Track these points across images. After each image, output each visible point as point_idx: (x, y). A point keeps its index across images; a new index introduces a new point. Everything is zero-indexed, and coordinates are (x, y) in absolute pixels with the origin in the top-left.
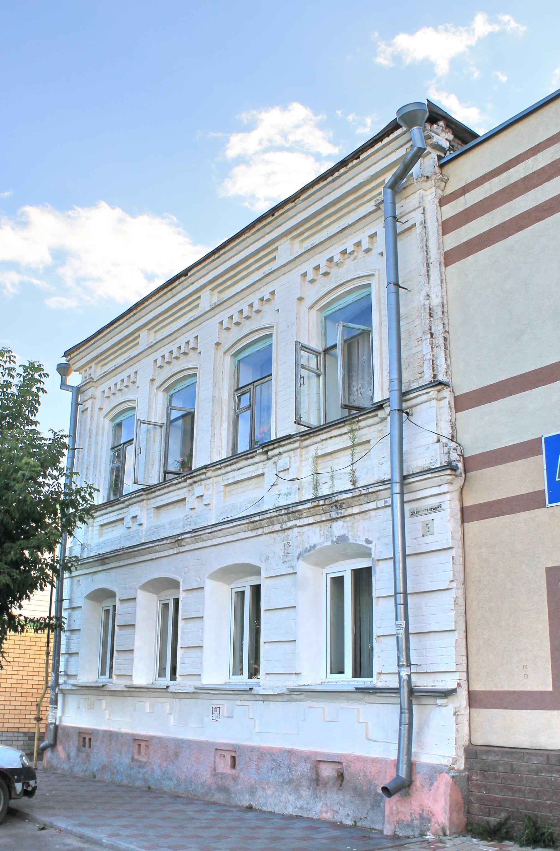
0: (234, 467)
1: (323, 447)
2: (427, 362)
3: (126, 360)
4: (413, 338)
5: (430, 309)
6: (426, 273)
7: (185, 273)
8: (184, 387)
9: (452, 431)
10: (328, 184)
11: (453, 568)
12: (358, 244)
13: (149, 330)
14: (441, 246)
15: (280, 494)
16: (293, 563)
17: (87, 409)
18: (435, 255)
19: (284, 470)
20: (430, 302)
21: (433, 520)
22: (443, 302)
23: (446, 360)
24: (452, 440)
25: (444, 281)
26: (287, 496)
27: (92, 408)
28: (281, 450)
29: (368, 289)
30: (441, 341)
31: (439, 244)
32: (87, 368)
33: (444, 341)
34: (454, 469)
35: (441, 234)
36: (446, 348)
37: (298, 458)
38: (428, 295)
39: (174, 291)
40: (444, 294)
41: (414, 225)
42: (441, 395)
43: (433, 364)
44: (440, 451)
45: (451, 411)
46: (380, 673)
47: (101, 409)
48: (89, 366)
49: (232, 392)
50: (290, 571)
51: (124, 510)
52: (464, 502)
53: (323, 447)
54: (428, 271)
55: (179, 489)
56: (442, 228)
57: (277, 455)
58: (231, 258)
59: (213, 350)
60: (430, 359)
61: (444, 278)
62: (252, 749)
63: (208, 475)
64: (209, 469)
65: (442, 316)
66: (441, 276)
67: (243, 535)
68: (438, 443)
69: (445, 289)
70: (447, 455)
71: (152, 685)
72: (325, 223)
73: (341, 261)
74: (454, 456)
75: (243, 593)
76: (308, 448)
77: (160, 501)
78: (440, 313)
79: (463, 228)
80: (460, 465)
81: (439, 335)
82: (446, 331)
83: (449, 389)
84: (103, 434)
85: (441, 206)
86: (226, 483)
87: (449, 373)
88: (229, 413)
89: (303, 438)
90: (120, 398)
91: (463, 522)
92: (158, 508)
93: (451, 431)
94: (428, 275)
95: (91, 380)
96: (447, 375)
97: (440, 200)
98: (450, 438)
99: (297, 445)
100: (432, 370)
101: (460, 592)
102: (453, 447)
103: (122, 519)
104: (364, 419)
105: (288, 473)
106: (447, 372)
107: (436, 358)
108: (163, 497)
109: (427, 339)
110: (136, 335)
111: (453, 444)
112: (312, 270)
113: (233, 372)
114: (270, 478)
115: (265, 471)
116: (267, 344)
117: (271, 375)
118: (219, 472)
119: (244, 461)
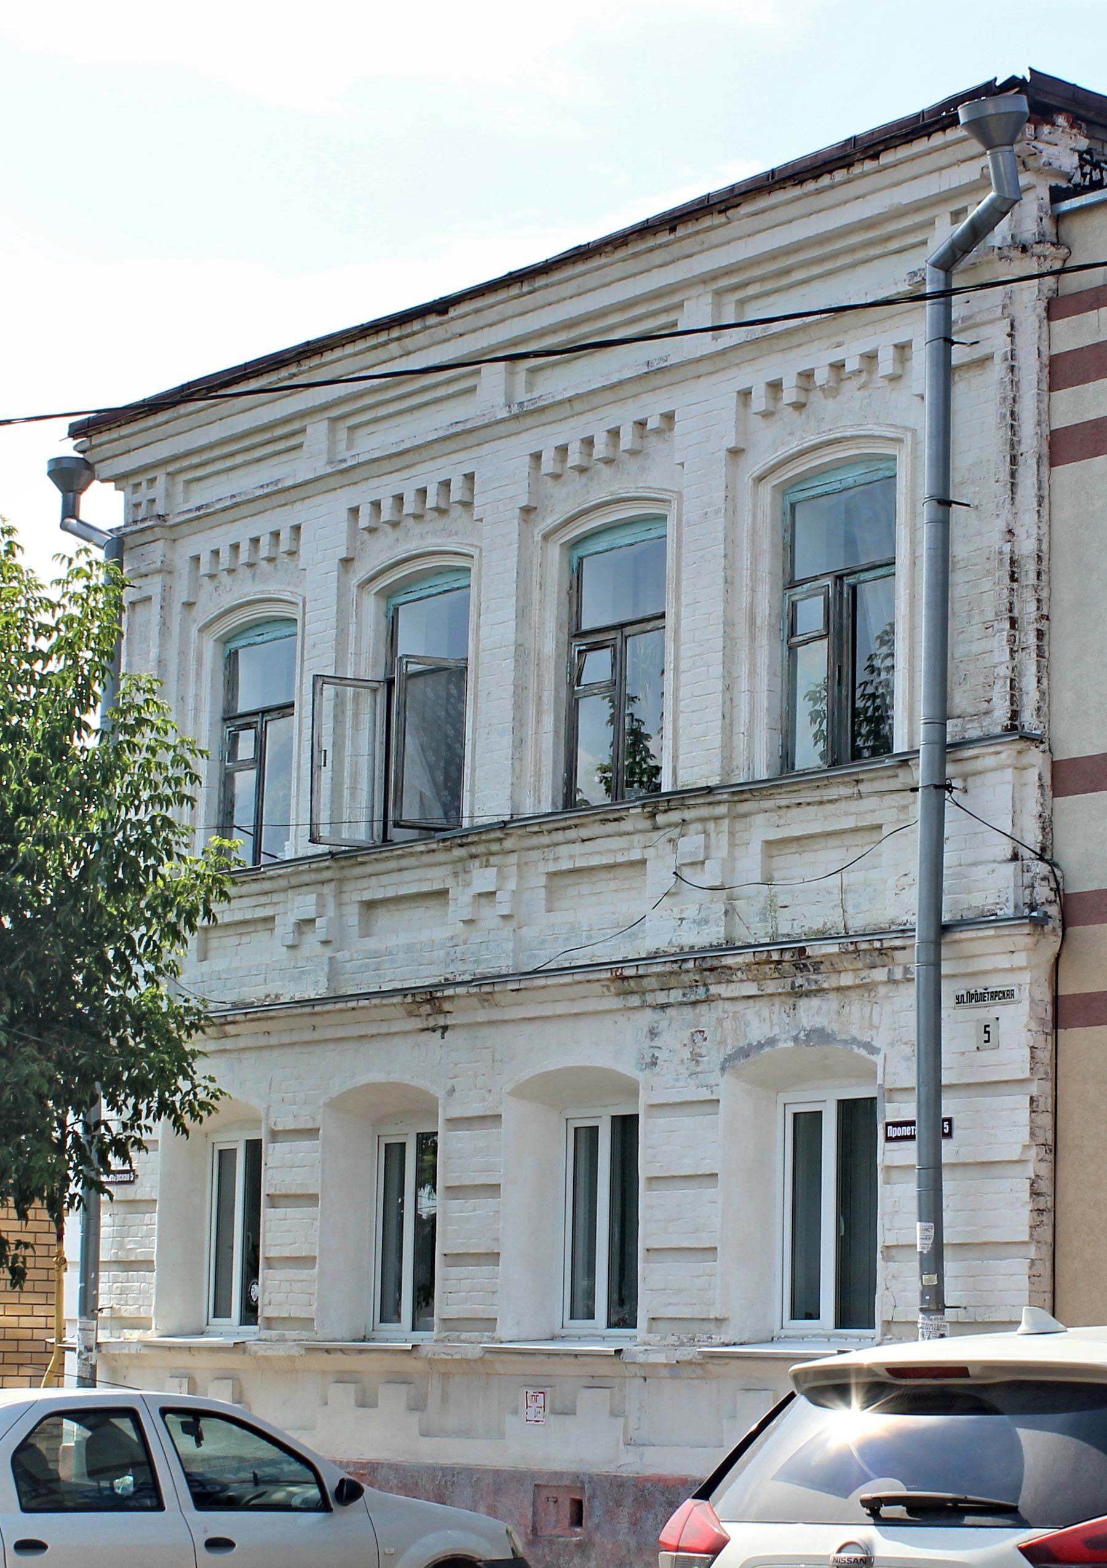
0: (572, 834)
1: (782, 822)
2: (1000, 682)
3: (266, 490)
4: (976, 619)
5: (1012, 562)
6: (1008, 478)
7: (441, 307)
8: (434, 591)
9: (1043, 836)
10: (807, 195)
11: (1032, 1121)
12: (871, 358)
13: (334, 420)
14: (1045, 417)
15: (684, 919)
16: (712, 1079)
17: (149, 599)
18: (1030, 441)
19: (693, 864)
20: (1013, 546)
21: (997, 1019)
22: (1040, 550)
23: (1039, 682)
24: (1041, 858)
25: (1046, 500)
26: (699, 924)
27: (163, 599)
28: (688, 814)
29: (890, 464)
30: (1031, 639)
31: (1039, 414)
32: (143, 478)
33: (1038, 639)
34: (1039, 923)
35: (1045, 387)
36: (1040, 654)
37: (724, 838)
38: (1010, 531)
39: (409, 343)
40: (1045, 529)
41: (989, 358)
42: (1026, 760)
43: (1012, 688)
44: (1015, 881)
45: (1042, 795)
46: (889, 1322)
47: (189, 605)
48: (150, 476)
49: (565, 638)
50: (705, 1095)
51: (276, 898)
52: (1059, 990)
53: (782, 822)
54: (1013, 475)
55: (430, 865)
56: (1050, 373)
57: (676, 825)
58: (565, 299)
59: (516, 521)
60: (1006, 677)
61: (1046, 493)
62: (617, 1484)
63: (508, 844)
64: (508, 831)
65: (1035, 582)
66: (1040, 489)
67: (592, 1005)
68: (1012, 865)
69: (1046, 518)
70: (1028, 891)
71: (363, 1341)
72: (797, 276)
73: (831, 384)
74: (1043, 892)
75: (594, 1130)
76: (748, 819)
77: (375, 890)
78: (1033, 575)
79: (1091, 386)
80: (1054, 910)
81: (1029, 623)
82: (1042, 617)
83: (1042, 747)
84: (198, 675)
85: (1050, 318)
86: (552, 867)
87: (1045, 709)
88: (557, 690)
89: (736, 799)
90: (246, 588)
91: (1056, 1026)
92: (370, 905)
93: (1041, 837)
94: (1012, 484)
95: (159, 522)
96: (1038, 716)
97: (1048, 303)
98: (1038, 851)
99: (722, 809)
100: (1008, 703)
101: (1045, 1169)
102: (1041, 875)
103: (270, 919)
104: (871, 780)
105: (703, 869)
106: (1039, 709)
107: (1020, 674)
108: (385, 879)
109: (1003, 630)
110: (296, 425)
111: (1042, 868)
112: (763, 387)
113: (566, 586)
114: (659, 875)
115: (649, 853)
116: (654, 534)
117: (662, 616)
118: (535, 841)
119: (597, 824)
